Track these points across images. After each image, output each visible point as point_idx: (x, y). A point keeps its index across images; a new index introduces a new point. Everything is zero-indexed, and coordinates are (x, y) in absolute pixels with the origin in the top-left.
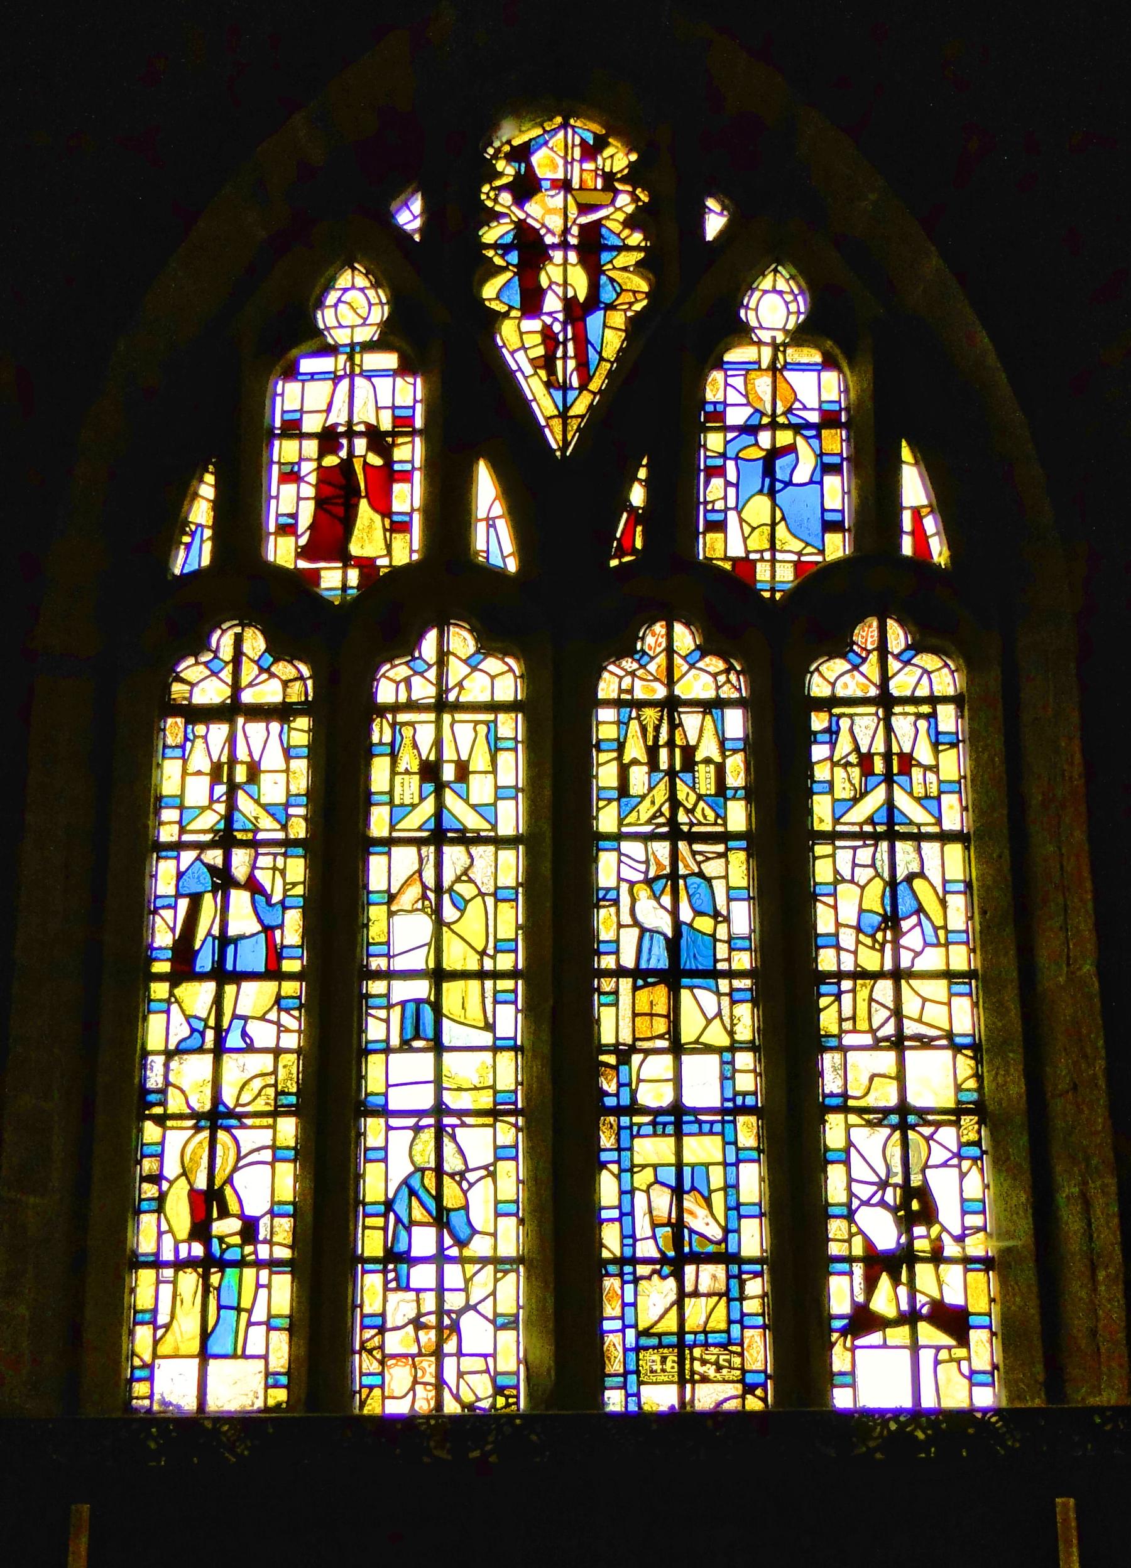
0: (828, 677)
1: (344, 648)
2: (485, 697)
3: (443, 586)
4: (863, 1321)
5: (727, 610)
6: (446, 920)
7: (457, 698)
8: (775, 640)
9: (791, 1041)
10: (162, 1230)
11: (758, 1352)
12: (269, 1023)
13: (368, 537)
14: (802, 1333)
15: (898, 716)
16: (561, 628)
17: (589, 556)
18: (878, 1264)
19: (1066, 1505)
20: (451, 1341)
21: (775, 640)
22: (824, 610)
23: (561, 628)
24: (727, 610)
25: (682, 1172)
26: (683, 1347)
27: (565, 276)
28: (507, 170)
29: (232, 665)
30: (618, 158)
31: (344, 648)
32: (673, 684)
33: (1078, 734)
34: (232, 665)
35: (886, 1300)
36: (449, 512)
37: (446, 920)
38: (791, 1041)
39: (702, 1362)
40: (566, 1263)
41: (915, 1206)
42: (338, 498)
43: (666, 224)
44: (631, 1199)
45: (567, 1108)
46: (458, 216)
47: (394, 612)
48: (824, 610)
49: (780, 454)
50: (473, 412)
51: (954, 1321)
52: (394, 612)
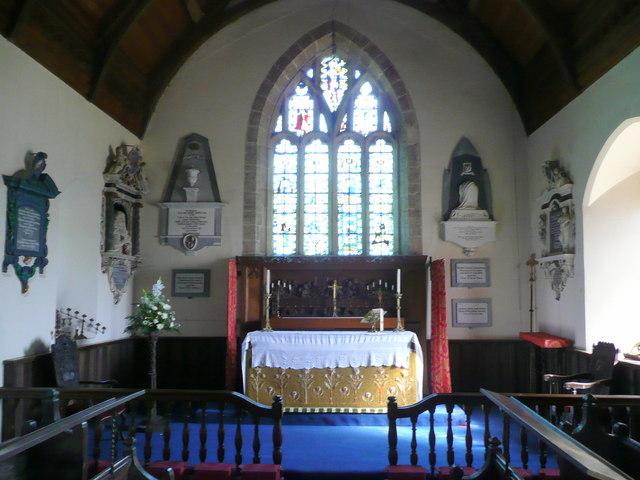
2: (358, 178)
3: (316, 133)
4: (374, 242)
6: (317, 184)
7: (317, 150)
8: (365, 142)
9: (365, 203)
10: (277, 229)
12: (292, 200)
14: (365, 243)
15: (383, 156)
16: (333, 138)
17: (337, 129)
18: (377, 235)
19: (399, 271)
20: (229, 464)
22: (372, 138)
23: (333, 138)
25: (350, 222)
26: (350, 247)
27: (334, 84)
28: (326, 66)
29: (285, 145)
30: (343, 63)
31: (300, 142)
32: (349, 150)
33: (257, 192)
34: (285, 145)
35: (378, 239)
37: (317, 184)
38: (365, 203)
39: (352, 248)
40: (333, 235)
41: (382, 227)
42: (300, 119)
43: (350, 74)
44: (343, 225)
45: (334, 213)
46: (318, 73)
48: (372, 138)
49: (367, 113)
50: (321, 106)
51: (387, 243)
52: (308, 138)
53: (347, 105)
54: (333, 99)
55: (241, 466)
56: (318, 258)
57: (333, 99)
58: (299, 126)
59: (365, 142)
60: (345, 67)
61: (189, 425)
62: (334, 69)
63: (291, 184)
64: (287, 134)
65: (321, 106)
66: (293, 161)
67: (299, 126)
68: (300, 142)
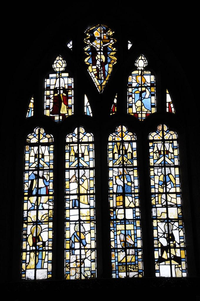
0: (153, 136)
1: (59, 131)
3: (78, 119)
4: (161, 260)
7: (81, 145)
8: (142, 128)
12: (47, 204)
13: (64, 110)
15: (165, 143)
16: (101, 129)
17: (106, 114)
23: (101, 129)
25: (126, 230)
31: (59, 131)
32: (124, 135)
41: (170, 237)
43: (120, 46)
46: (79, 45)
50: (83, 84)
51: (178, 260)
53: (119, 83)
54: (98, 74)
56: (53, 174)
57: (98, 74)
58: (56, 110)
59: (142, 128)
61: (24, 209)
62: (99, 37)
63: (45, 184)
64: (40, 120)
66: (48, 154)
67: (56, 110)
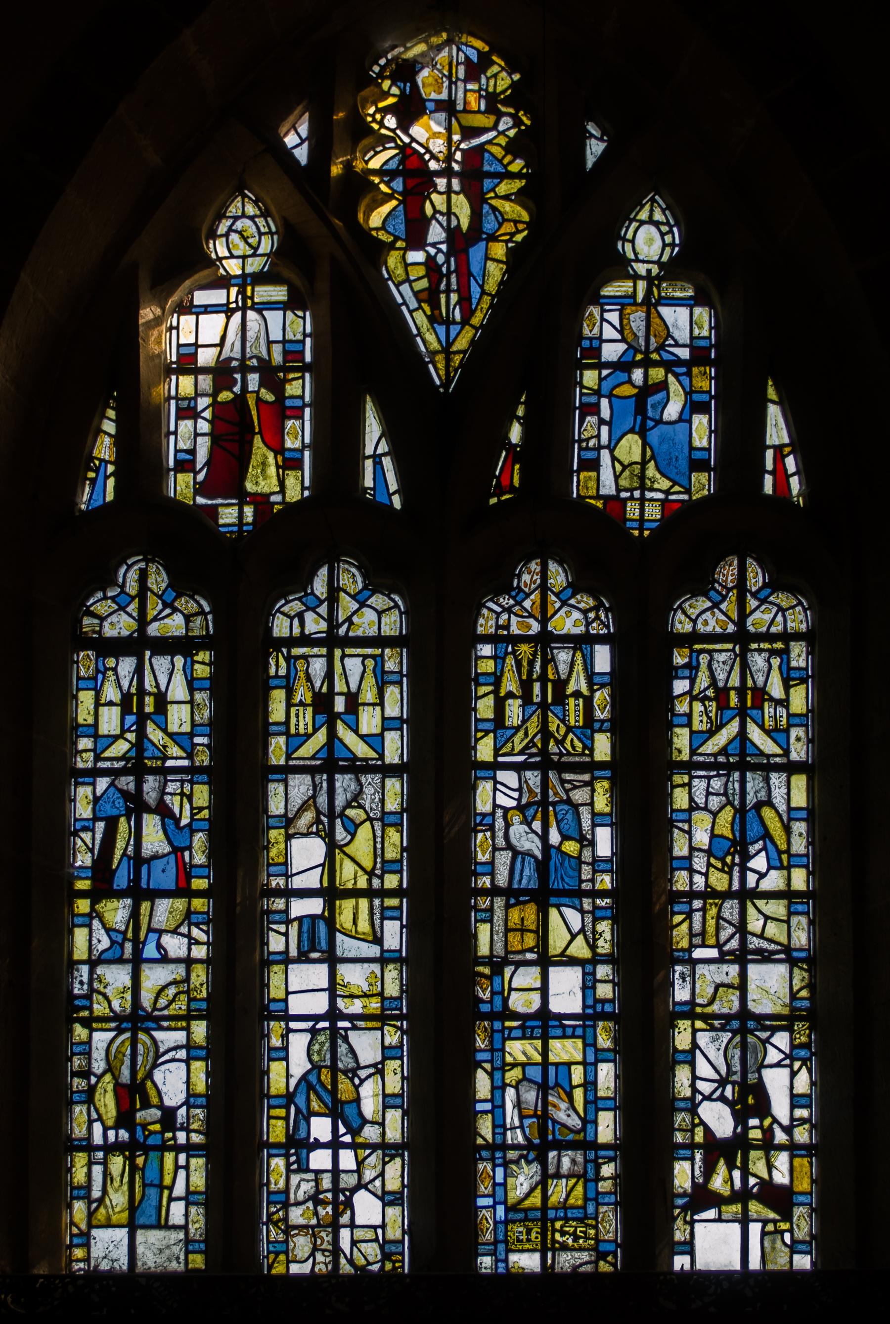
0: (695, 615)
3: (332, 523)
5: (599, 549)
8: (641, 576)
10: (93, 1120)
11: (610, 1225)
13: (264, 477)
16: (444, 555)
17: (458, 489)
18: (717, 1150)
21: (641, 576)
22: (688, 549)
23: (444, 555)
24: (599, 549)
31: (240, 579)
32: (549, 609)
36: (337, 448)
41: (750, 1100)
43: (545, 150)
47: (287, 549)
48: (688, 549)
49: (651, 391)
50: (359, 346)
52: (287, 549)
55: (142, 565)
58: (227, 472)
60: (518, 97)
62: (441, 116)
64: (152, 524)
65: (163, 811)
67: (227, 472)
68: (240, 579)
